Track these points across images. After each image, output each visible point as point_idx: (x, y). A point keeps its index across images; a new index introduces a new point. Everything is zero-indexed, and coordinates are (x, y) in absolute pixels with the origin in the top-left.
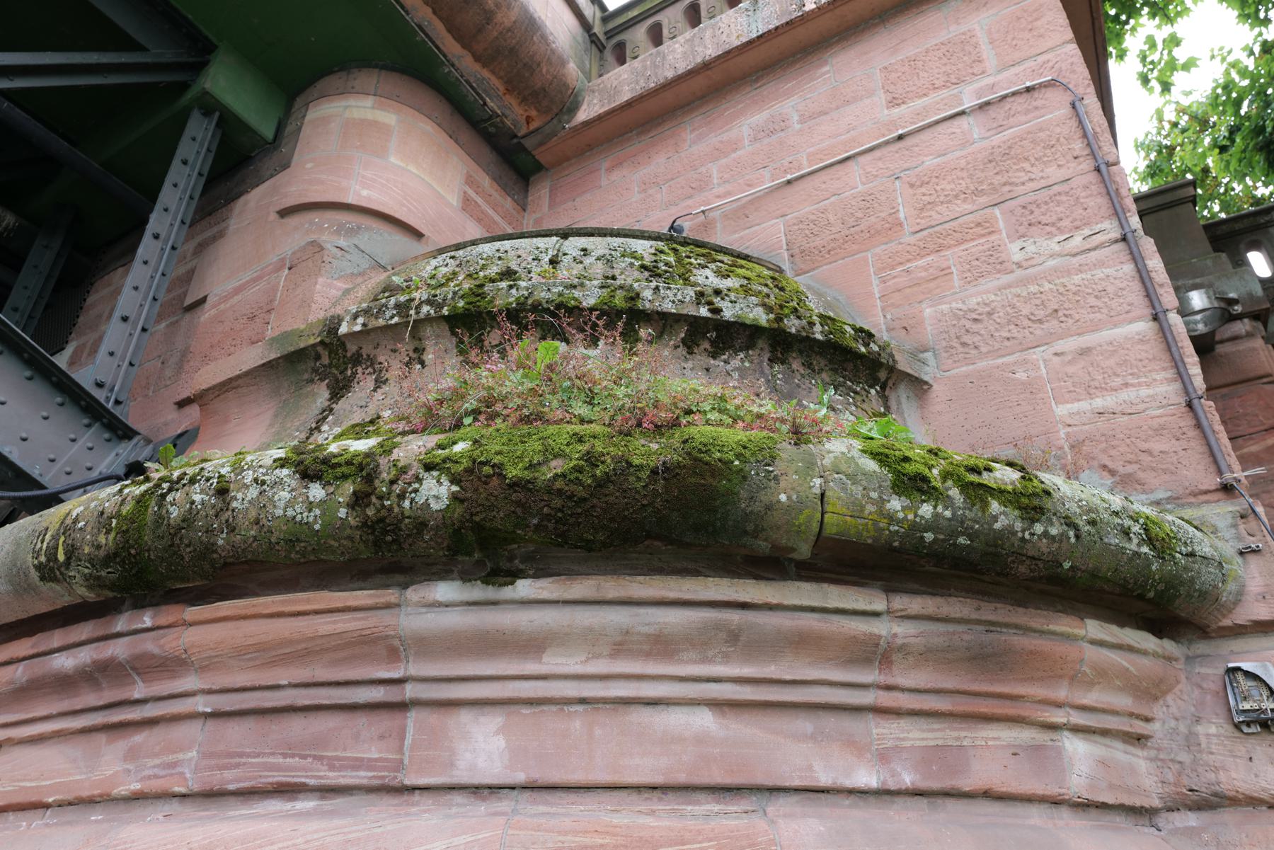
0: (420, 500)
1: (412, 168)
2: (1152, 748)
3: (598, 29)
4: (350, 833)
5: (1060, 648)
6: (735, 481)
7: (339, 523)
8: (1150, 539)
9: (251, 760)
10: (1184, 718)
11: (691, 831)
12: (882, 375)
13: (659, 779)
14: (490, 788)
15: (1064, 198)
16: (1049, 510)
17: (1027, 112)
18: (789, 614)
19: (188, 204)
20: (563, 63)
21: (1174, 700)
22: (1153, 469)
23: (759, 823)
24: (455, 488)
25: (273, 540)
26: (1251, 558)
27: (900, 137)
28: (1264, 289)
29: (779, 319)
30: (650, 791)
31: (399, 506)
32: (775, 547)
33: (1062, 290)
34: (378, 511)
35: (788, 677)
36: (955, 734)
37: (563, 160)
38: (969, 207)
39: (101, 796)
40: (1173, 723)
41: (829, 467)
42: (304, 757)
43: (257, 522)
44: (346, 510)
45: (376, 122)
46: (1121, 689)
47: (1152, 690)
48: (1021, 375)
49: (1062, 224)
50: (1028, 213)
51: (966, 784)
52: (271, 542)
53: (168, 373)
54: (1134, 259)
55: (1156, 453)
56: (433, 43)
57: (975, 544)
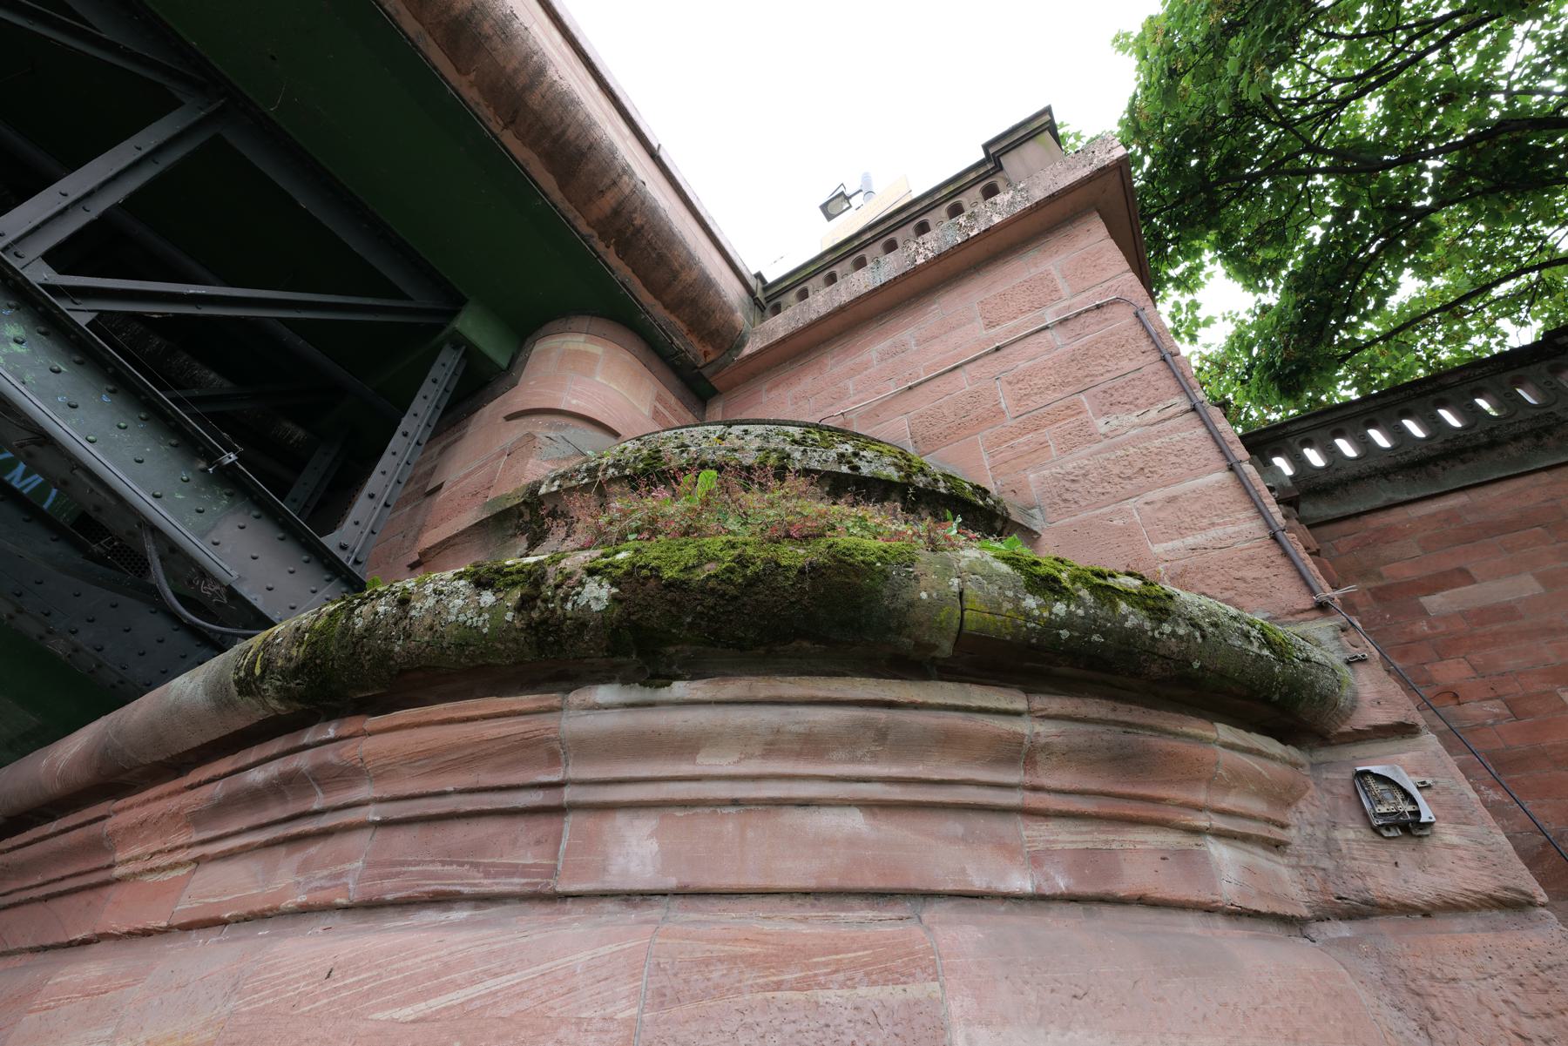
0: (582, 602)
1: (613, 385)
2: (1292, 855)
3: (759, 295)
4: (495, 943)
5: (1196, 750)
6: (877, 580)
7: (505, 625)
8: (1269, 643)
9: (411, 868)
10: (1319, 824)
11: (845, 939)
12: (998, 525)
13: (812, 884)
14: (642, 895)
15: (1138, 383)
16: (1174, 612)
17: (1099, 323)
18: (934, 713)
19: (434, 412)
20: (732, 312)
21: (1307, 807)
22: (1249, 594)
23: (917, 931)
24: (614, 590)
25: (445, 645)
26: (1357, 666)
27: (998, 349)
28: (1293, 483)
29: (909, 476)
30: (803, 897)
31: (562, 608)
32: (919, 645)
33: (1145, 452)
34: (542, 613)
35: (936, 777)
36: (1103, 837)
37: (733, 386)
38: (1058, 395)
39: (271, 910)
40: (1309, 830)
41: (965, 568)
42: (461, 864)
43: (431, 628)
44: (512, 614)
45: (586, 352)
46: (1256, 794)
47: (1285, 796)
48: (1118, 522)
49: (1139, 402)
50: (1108, 395)
51: (1122, 889)
52: (442, 647)
53: (407, 544)
54: (1205, 424)
55: (1250, 580)
56: (633, 296)
57: (1109, 642)
